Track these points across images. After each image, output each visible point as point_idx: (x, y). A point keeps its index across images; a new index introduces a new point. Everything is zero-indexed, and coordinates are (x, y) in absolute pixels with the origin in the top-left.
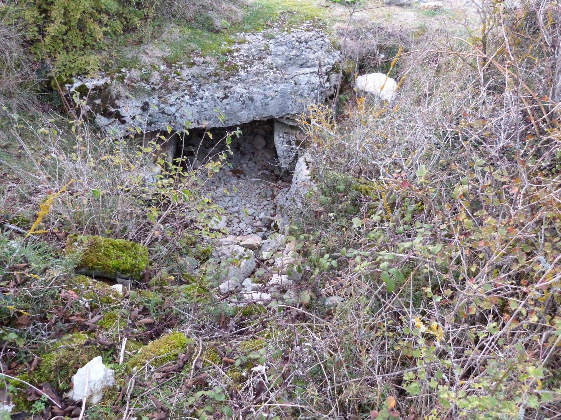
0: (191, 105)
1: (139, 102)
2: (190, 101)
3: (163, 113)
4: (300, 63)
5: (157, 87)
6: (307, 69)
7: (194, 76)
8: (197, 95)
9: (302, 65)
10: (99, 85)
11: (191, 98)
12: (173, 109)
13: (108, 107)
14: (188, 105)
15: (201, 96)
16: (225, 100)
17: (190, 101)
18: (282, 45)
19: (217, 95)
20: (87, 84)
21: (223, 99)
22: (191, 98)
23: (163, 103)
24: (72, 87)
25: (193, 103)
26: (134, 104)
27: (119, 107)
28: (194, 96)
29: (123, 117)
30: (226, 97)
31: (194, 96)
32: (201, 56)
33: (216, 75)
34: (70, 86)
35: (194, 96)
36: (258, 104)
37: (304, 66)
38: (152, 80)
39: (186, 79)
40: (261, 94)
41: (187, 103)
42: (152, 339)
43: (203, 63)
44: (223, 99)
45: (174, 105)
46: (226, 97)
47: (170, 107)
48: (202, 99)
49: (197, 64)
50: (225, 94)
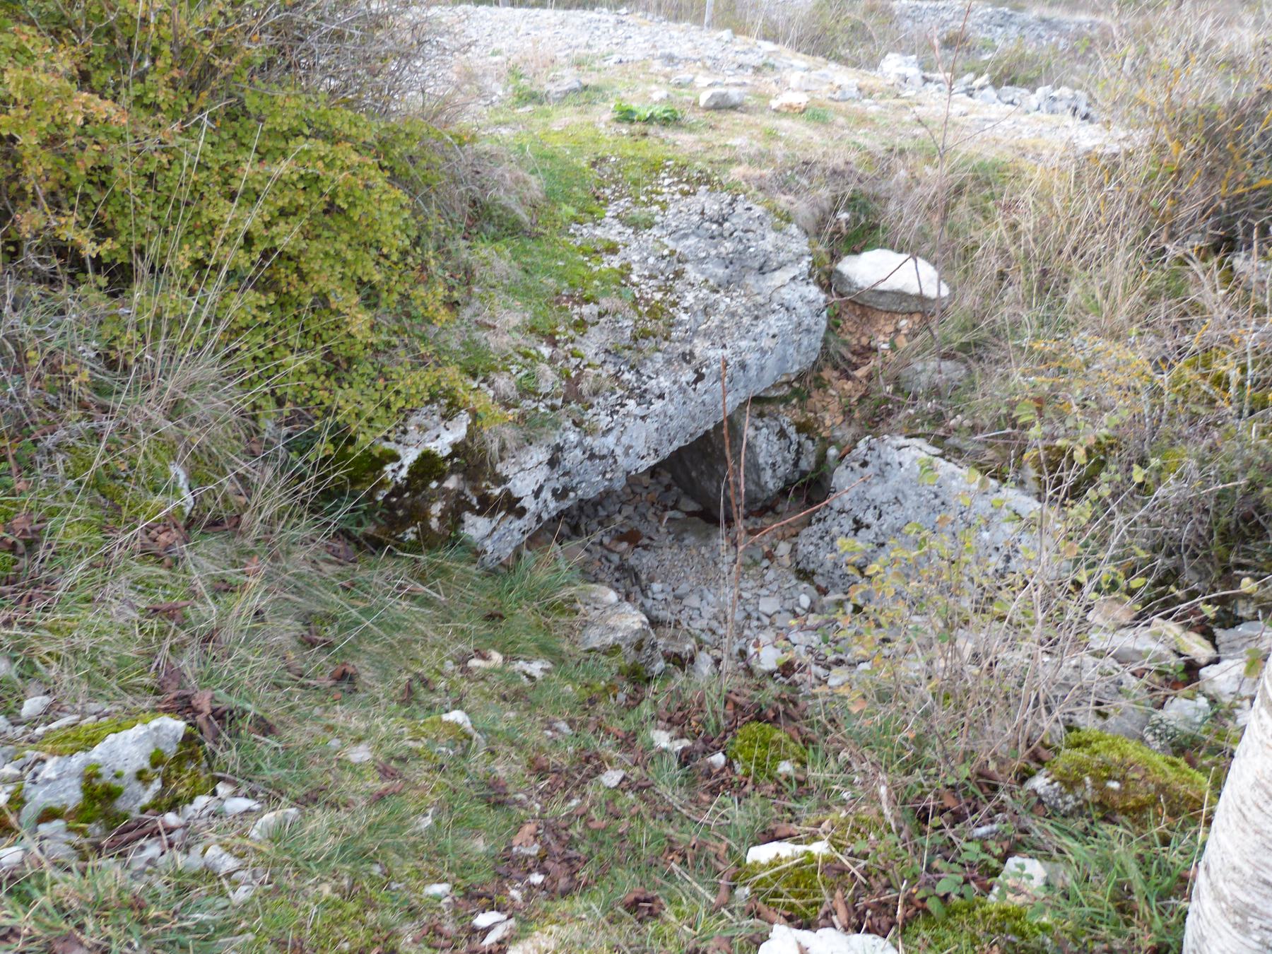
0: (643, 418)
1: (543, 449)
2: (639, 411)
3: (592, 457)
4: (757, 265)
5: (559, 402)
6: (777, 274)
7: (607, 351)
8: (645, 391)
9: (761, 268)
10: (459, 440)
11: (639, 404)
12: (610, 440)
13: (488, 487)
14: (639, 421)
15: (657, 392)
16: (699, 385)
17: (639, 411)
18: (686, 236)
19: (684, 379)
20: (432, 446)
21: (696, 382)
22: (639, 404)
23: (587, 433)
24: (401, 467)
25: (647, 412)
26: (535, 460)
27: (505, 480)
28: (641, 396)
29: (520, 499)
30: (700, 377)
31: (641, 396)
32: (587, 301)
33: (645, 335)
34: (396, 466)
35: (642, 396)
36: (753, 372)
37: (765, 269)
38: (544, 387)
39: (598, 362)
40: (754, 350)
41: (635, 417)
42: (60, 755)
43: (601, 315)
44: (696, 382)
45: (610, 430)
46: (700, 377)
47: (603, 439)
48: (661, 396)
49: (590, 320)
50: (696, 371)
